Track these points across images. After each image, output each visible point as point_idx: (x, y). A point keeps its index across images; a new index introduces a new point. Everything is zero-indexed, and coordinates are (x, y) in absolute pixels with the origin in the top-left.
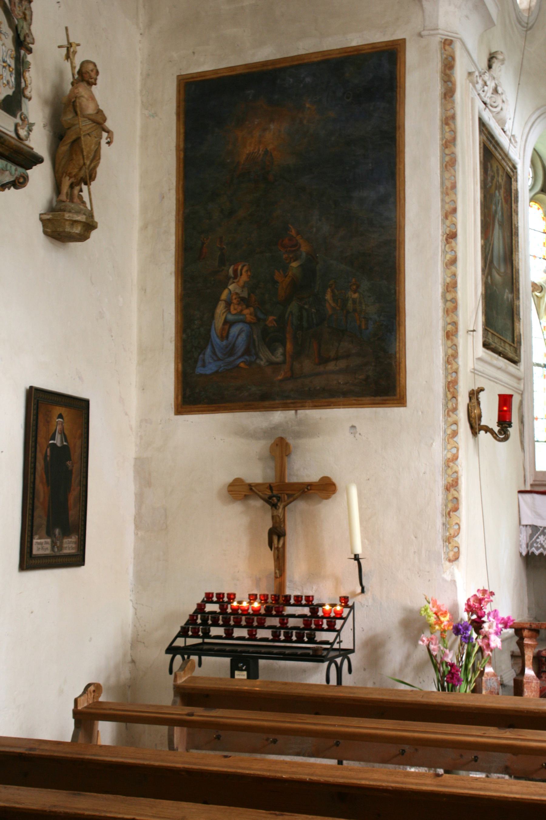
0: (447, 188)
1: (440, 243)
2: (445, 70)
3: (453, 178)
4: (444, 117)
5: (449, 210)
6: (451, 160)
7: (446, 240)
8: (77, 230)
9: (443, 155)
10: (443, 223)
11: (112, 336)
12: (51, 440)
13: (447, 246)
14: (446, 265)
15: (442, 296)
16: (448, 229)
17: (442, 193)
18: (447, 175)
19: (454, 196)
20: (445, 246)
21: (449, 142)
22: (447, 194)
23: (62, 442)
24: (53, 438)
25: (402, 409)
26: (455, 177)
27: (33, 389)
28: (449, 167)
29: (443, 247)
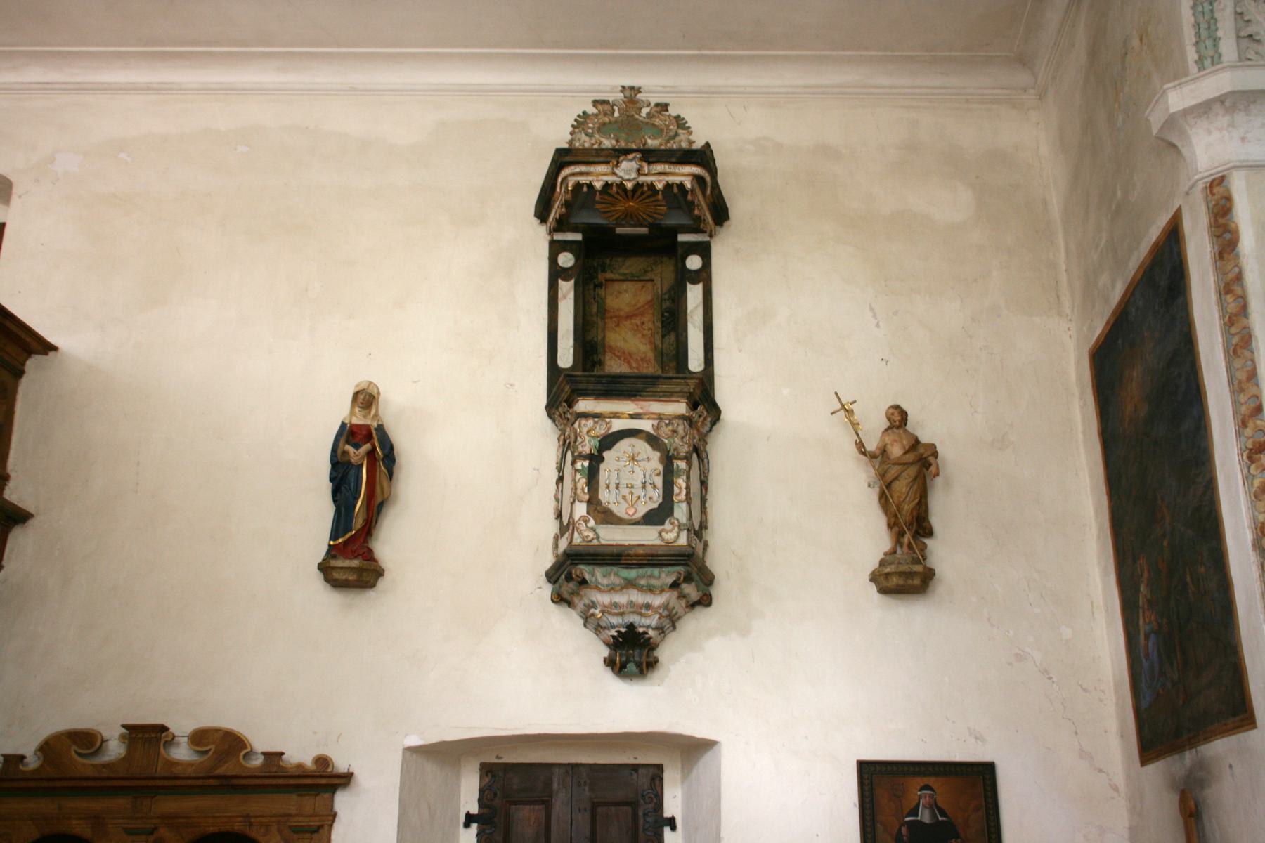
0: (1240, 382)
1: (1238, 467)
2: (1216, 221)
3: (1249, 363)
4: (1222, 285)
5: (1247, 413)
6: (1242, 339)
7: (1249, 458)
8: (917, 582)
9: (1227, 335)
10: (1239, 434)
11: (1050, 678)
12: (909, 815)
13: (1253, 467)
14: (1255, 496)
15: (1254, 545)
16: (1251, 441)
17: (1232, 392)
18: (1238, 363)
19: (1255, 388)
20: (1249, 468)
21: (1236, 315)
22: (1242, 390)
23: (933, 815)
24: (914, 812)
25: (1254, 731)
26: (1252, 360)
27: (310, 803)
28: (1239, 351)
29: (1245, 471)
